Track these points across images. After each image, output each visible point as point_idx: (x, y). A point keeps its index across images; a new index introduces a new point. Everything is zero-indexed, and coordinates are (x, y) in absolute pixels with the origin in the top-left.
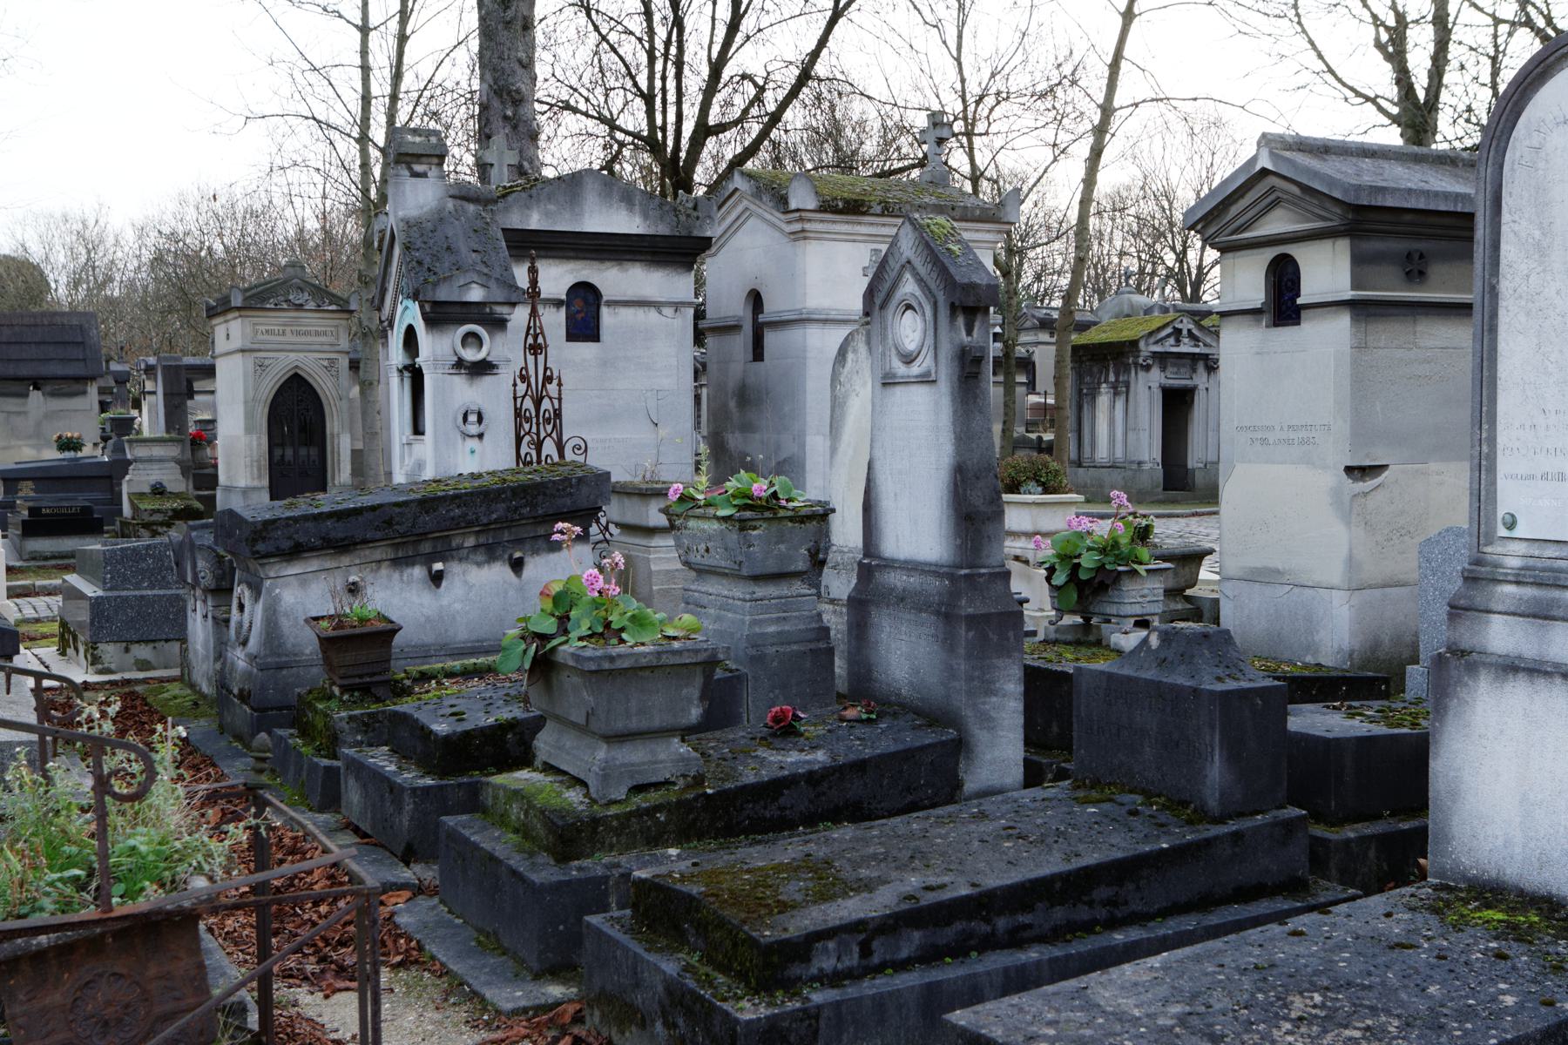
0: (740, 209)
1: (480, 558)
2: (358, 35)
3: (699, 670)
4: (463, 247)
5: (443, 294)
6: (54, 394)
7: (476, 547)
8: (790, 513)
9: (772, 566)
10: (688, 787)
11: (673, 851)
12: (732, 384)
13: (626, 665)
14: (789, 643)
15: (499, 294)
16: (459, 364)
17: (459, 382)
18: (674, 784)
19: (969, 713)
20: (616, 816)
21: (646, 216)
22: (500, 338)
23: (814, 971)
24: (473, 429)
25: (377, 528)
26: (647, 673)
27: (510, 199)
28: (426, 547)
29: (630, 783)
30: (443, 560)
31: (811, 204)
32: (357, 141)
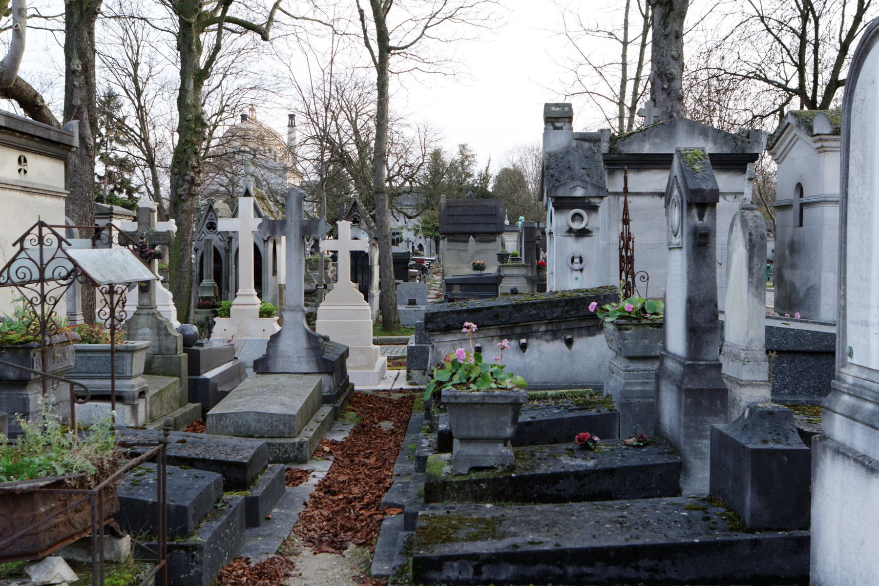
0: (792, 135)
1: (548, 337)
2: (621, 46)
3: (510, 407)
4: (577, 167)
5: (561, 193)
6: (480, 241)
7: (546, 332)
8: (649, 322)
9: (639, 352)
10: (505, 471)
11: (488, 506)
12: (787, 240)
13: (464, 401)
14: (648, 398)
15: (592, 192)
16: (570, 230)
17: (570, 241)
18: (496, 469)
19: (687, 448)
20: (457, 482)
21: (715, 143)
22: (593, 216)
23: (444, 577)
24: (577, 266)
25: (490, 319)
26: (479, 407)
27: (632, 137)
28: (518, 330)
29: (470, 465)
30: (527, 338)
31: (827, 130)
32: (618, 104)
